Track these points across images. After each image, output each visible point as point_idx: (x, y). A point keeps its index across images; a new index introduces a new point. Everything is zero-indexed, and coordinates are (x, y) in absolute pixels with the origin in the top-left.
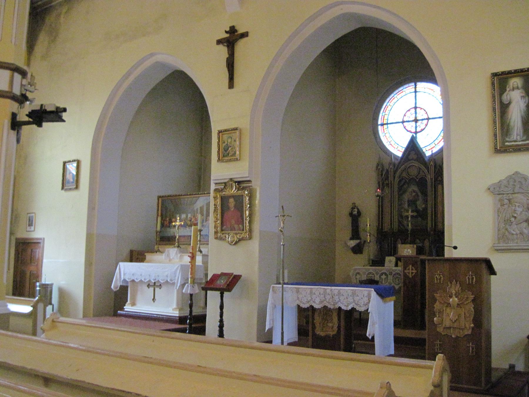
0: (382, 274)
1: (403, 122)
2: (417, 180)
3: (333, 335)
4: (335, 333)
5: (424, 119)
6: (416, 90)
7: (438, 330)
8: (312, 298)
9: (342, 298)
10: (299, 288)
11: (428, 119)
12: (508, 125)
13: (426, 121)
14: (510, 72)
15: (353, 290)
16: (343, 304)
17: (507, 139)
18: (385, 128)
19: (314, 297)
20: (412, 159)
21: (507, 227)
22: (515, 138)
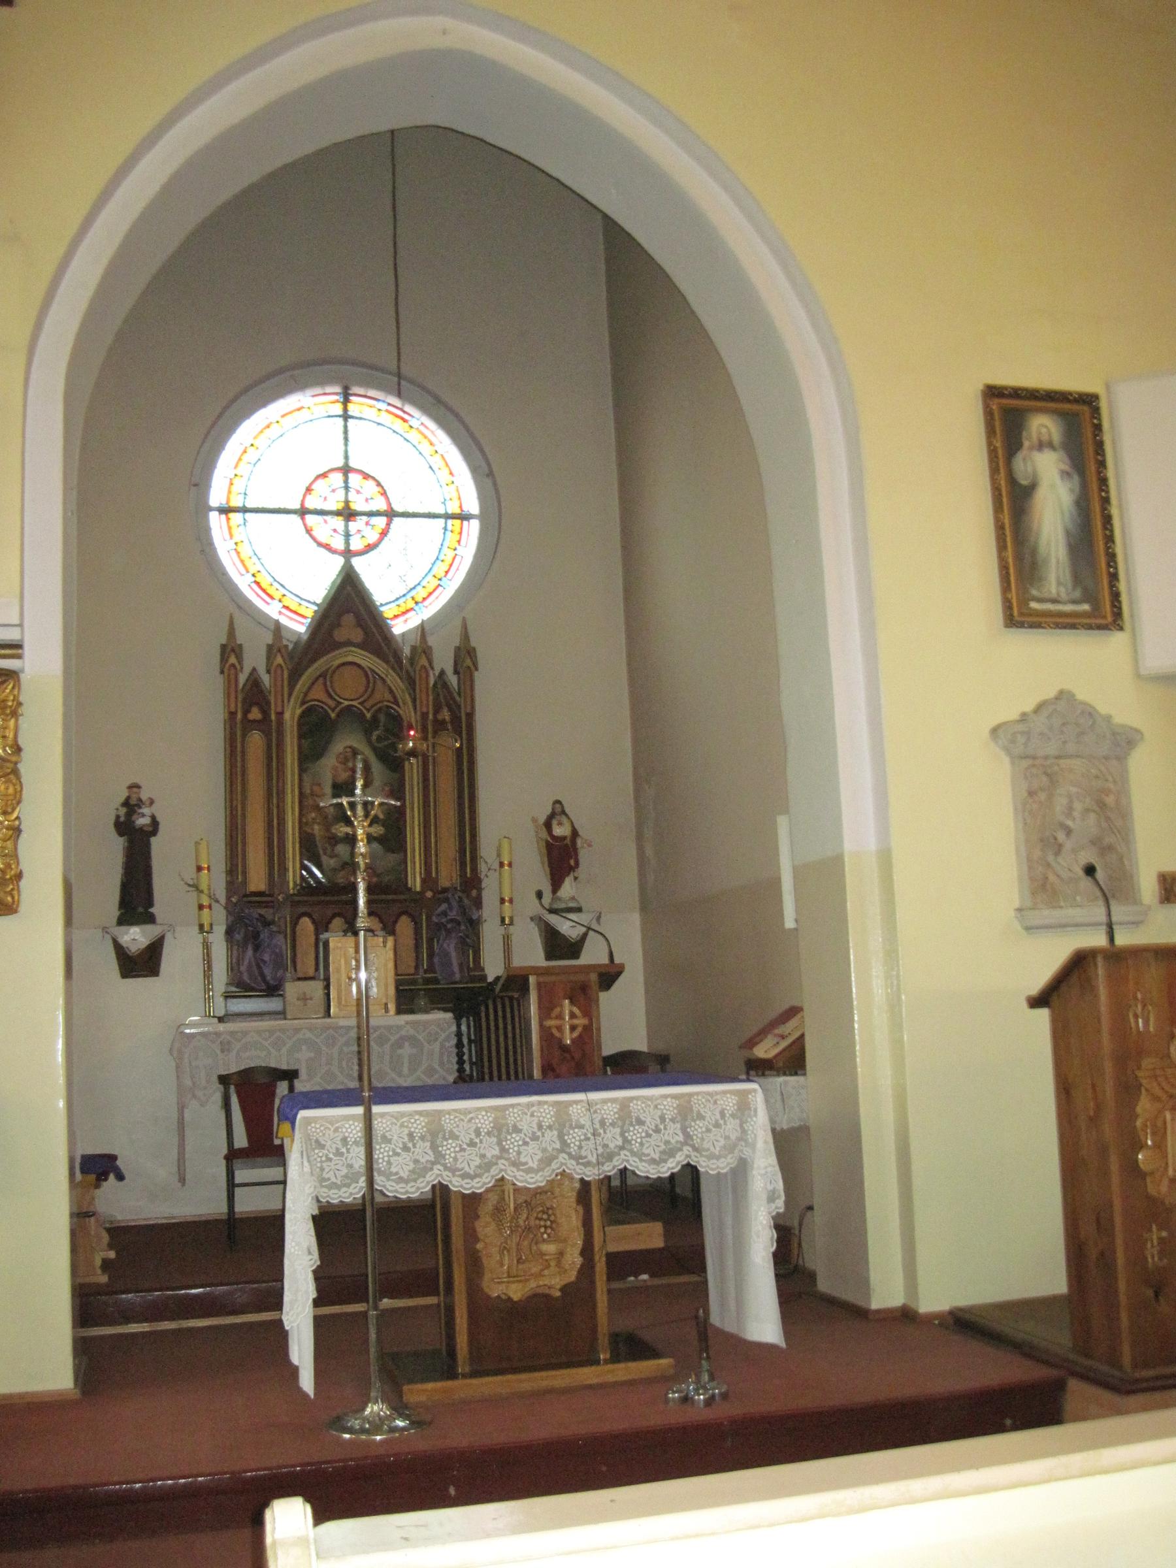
0: (399, 1044)
1: (303, 512)
2: (368, 715)
3: (563, 1289)
5: (378, 514)
6: (345, 410)
7: (1151, 1190)
8: (503, 1150)
9: (635, 1134)
10: (440, 1113)
11: (390, 514)
12: (1034, 552)
13: (381, 522)
15: (682, 1096)
16: (640, 1156)
17: (1034, 592)
18: (232, 523)
19: (635, 1134)
20: (349, 643)
21: (1051, 858)
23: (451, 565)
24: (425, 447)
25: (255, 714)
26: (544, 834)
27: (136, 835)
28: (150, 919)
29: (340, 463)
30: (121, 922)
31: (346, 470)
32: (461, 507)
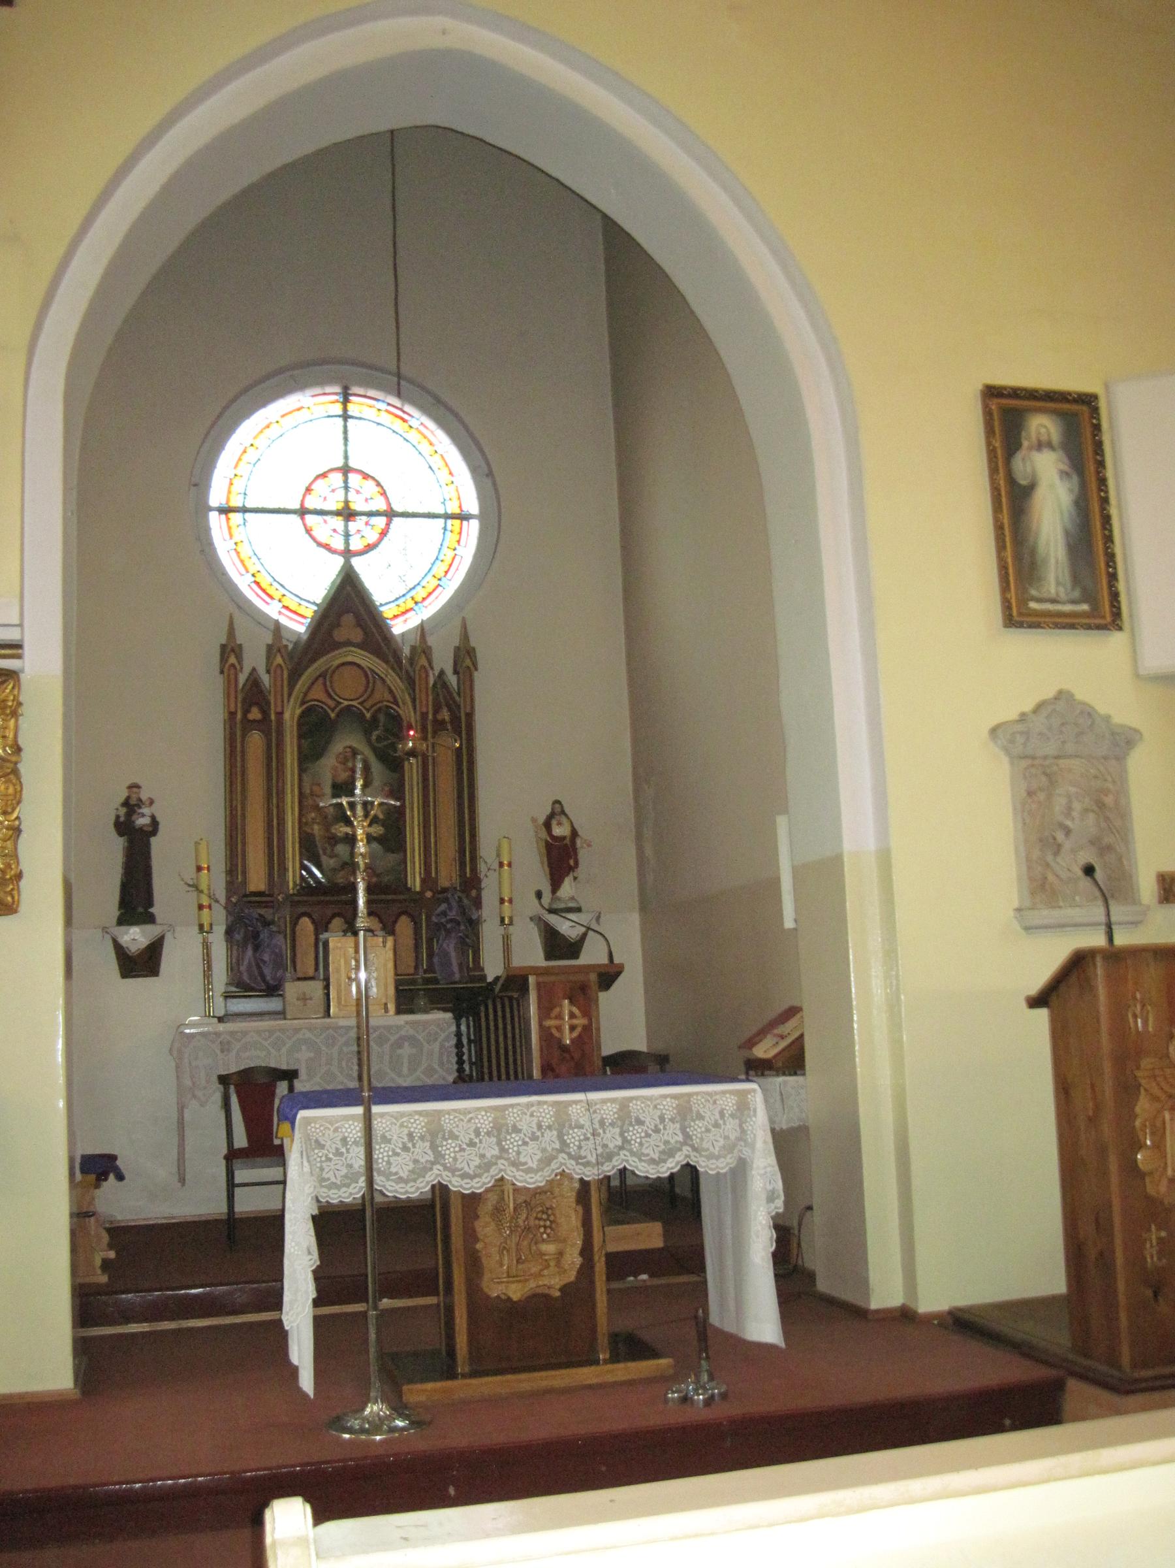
0: (398, 1044)
1: (303, 512)
2: (368, 715)
4: (572, 1276)
6: (345, 409)
7: (1150, 1190)
8: (503, 1150)
9: (635, 1134)
10: (439, 1113)
11: (390, 514)
12: (1033, 552)
13: (381, 521)
14: (1033, 395)
16: (640, 1156)
17: (1033, 592)
19: (635, 1134)
20: (348, 643)
21: (1050, 858)
22: (1053, 591)
23: (451, 565)
24: (425, 447)
25: (255, 714)
26: (544, 834)
27: (136, 835)
28: (150, 919)
29: (340, 463)
30: (121, 922)
31: (346, 470)
32: (460, 507)
